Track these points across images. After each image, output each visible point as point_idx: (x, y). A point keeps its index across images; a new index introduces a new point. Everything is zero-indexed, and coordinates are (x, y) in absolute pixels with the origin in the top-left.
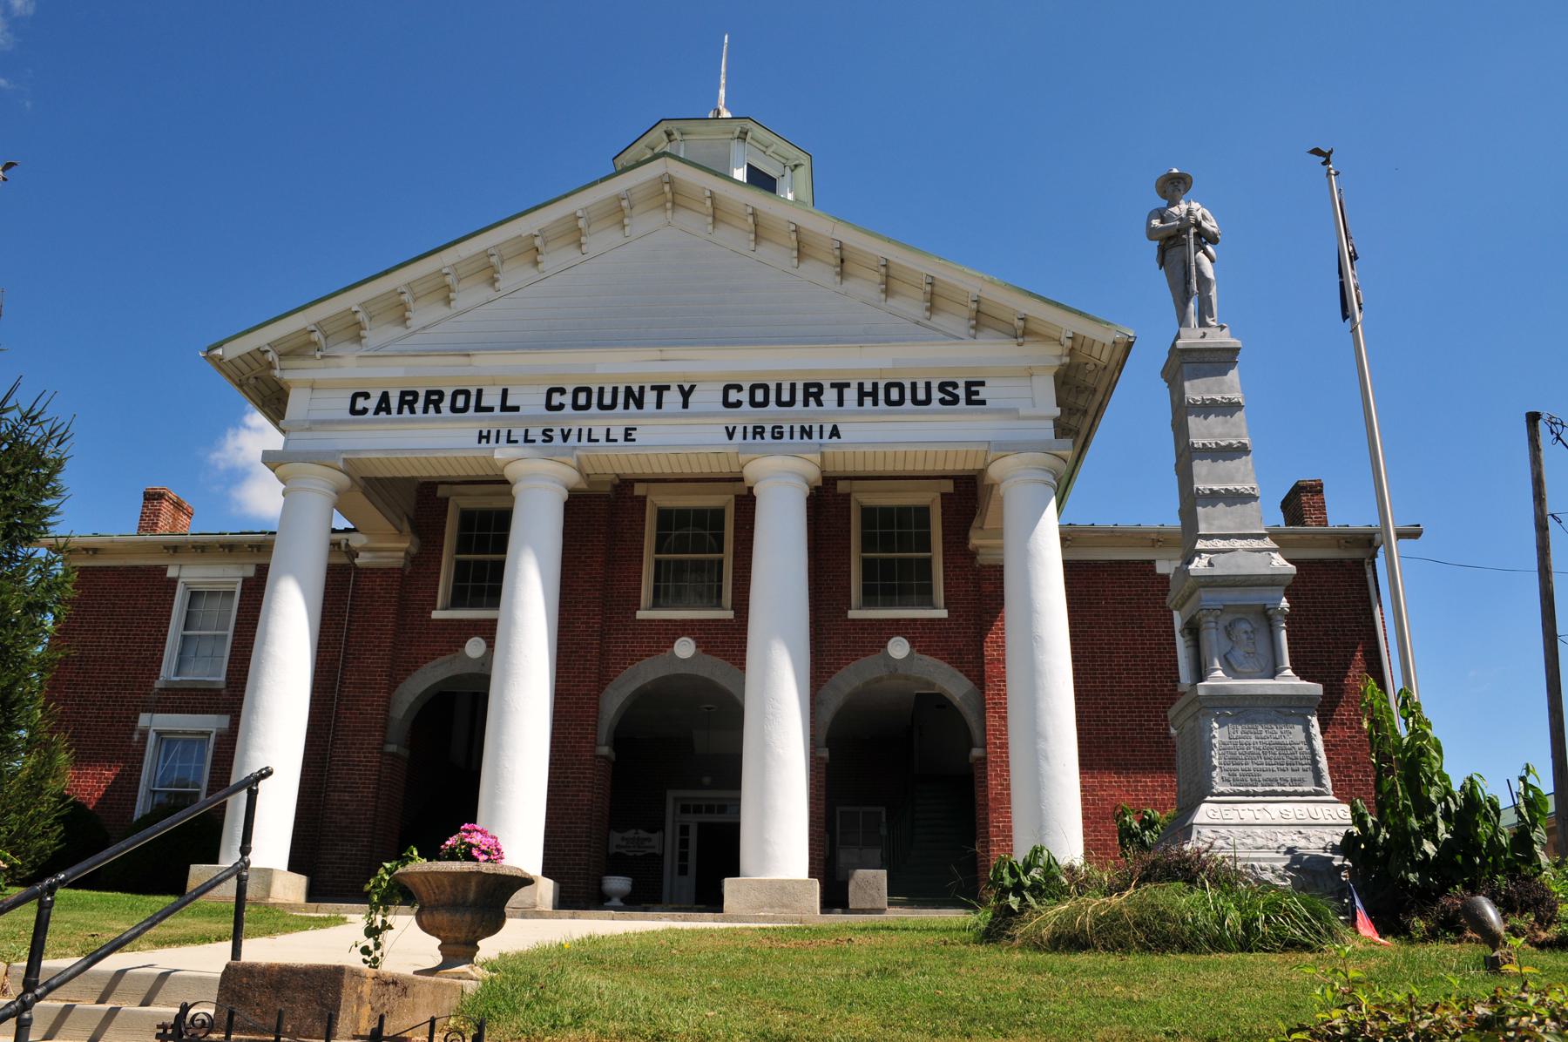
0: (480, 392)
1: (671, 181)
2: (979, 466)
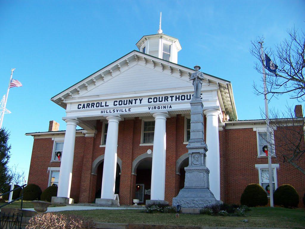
0: (101, 103)
1: (137, 56)
2: (184, 116)
